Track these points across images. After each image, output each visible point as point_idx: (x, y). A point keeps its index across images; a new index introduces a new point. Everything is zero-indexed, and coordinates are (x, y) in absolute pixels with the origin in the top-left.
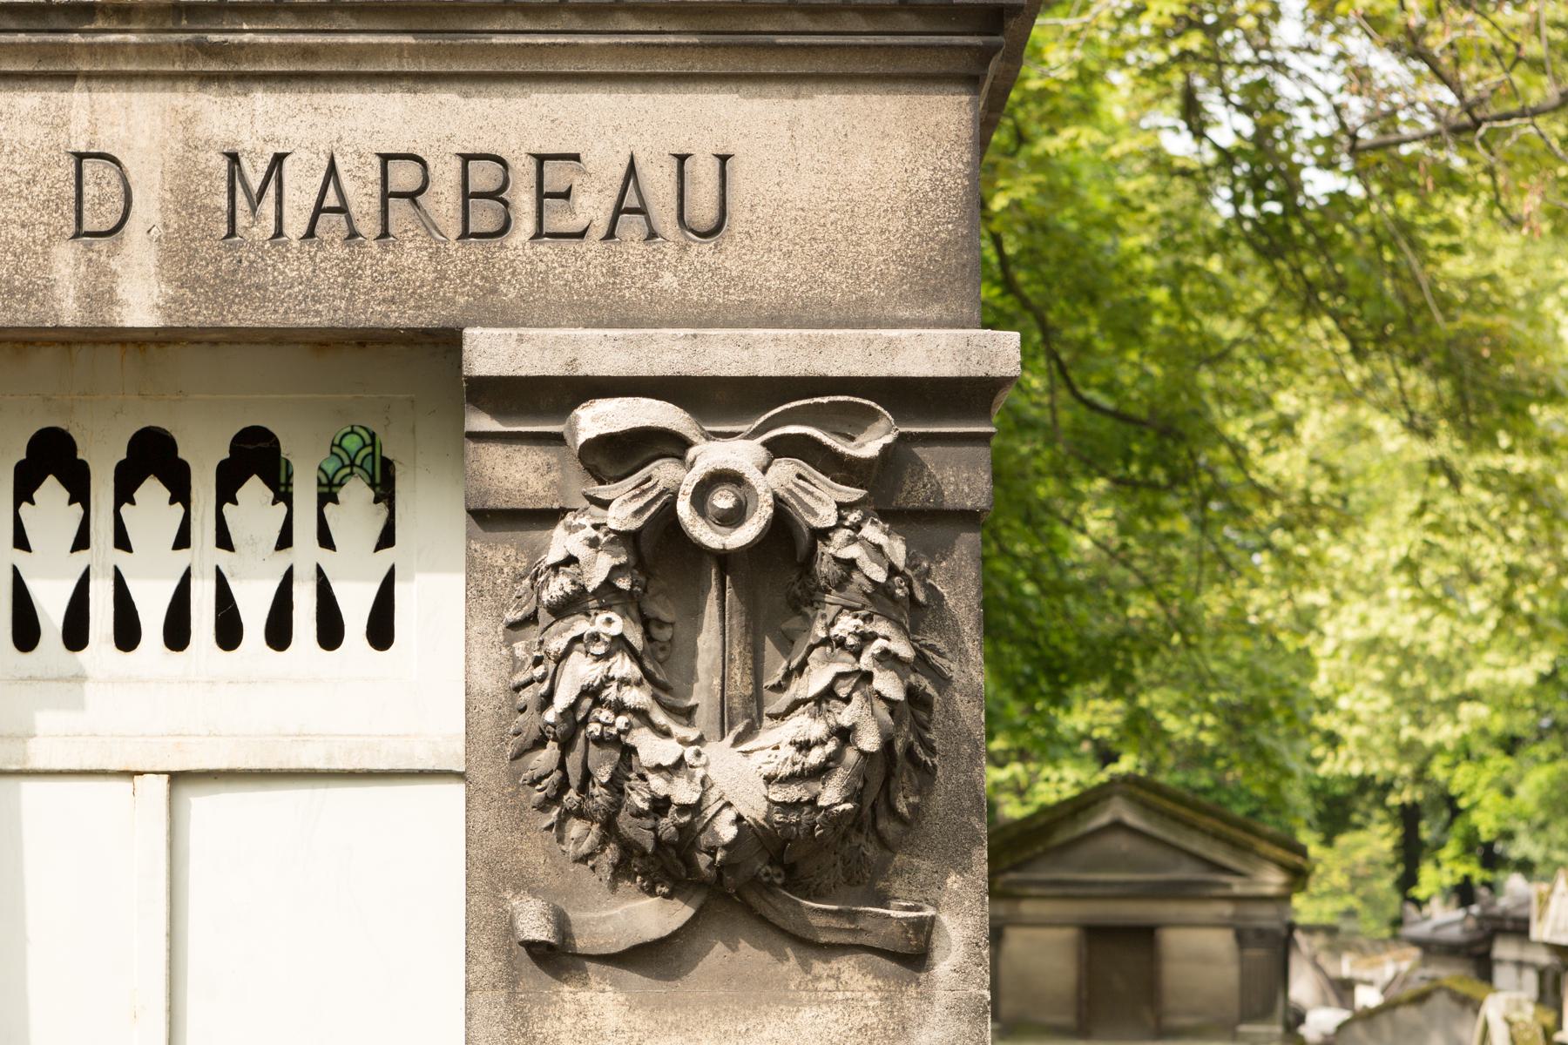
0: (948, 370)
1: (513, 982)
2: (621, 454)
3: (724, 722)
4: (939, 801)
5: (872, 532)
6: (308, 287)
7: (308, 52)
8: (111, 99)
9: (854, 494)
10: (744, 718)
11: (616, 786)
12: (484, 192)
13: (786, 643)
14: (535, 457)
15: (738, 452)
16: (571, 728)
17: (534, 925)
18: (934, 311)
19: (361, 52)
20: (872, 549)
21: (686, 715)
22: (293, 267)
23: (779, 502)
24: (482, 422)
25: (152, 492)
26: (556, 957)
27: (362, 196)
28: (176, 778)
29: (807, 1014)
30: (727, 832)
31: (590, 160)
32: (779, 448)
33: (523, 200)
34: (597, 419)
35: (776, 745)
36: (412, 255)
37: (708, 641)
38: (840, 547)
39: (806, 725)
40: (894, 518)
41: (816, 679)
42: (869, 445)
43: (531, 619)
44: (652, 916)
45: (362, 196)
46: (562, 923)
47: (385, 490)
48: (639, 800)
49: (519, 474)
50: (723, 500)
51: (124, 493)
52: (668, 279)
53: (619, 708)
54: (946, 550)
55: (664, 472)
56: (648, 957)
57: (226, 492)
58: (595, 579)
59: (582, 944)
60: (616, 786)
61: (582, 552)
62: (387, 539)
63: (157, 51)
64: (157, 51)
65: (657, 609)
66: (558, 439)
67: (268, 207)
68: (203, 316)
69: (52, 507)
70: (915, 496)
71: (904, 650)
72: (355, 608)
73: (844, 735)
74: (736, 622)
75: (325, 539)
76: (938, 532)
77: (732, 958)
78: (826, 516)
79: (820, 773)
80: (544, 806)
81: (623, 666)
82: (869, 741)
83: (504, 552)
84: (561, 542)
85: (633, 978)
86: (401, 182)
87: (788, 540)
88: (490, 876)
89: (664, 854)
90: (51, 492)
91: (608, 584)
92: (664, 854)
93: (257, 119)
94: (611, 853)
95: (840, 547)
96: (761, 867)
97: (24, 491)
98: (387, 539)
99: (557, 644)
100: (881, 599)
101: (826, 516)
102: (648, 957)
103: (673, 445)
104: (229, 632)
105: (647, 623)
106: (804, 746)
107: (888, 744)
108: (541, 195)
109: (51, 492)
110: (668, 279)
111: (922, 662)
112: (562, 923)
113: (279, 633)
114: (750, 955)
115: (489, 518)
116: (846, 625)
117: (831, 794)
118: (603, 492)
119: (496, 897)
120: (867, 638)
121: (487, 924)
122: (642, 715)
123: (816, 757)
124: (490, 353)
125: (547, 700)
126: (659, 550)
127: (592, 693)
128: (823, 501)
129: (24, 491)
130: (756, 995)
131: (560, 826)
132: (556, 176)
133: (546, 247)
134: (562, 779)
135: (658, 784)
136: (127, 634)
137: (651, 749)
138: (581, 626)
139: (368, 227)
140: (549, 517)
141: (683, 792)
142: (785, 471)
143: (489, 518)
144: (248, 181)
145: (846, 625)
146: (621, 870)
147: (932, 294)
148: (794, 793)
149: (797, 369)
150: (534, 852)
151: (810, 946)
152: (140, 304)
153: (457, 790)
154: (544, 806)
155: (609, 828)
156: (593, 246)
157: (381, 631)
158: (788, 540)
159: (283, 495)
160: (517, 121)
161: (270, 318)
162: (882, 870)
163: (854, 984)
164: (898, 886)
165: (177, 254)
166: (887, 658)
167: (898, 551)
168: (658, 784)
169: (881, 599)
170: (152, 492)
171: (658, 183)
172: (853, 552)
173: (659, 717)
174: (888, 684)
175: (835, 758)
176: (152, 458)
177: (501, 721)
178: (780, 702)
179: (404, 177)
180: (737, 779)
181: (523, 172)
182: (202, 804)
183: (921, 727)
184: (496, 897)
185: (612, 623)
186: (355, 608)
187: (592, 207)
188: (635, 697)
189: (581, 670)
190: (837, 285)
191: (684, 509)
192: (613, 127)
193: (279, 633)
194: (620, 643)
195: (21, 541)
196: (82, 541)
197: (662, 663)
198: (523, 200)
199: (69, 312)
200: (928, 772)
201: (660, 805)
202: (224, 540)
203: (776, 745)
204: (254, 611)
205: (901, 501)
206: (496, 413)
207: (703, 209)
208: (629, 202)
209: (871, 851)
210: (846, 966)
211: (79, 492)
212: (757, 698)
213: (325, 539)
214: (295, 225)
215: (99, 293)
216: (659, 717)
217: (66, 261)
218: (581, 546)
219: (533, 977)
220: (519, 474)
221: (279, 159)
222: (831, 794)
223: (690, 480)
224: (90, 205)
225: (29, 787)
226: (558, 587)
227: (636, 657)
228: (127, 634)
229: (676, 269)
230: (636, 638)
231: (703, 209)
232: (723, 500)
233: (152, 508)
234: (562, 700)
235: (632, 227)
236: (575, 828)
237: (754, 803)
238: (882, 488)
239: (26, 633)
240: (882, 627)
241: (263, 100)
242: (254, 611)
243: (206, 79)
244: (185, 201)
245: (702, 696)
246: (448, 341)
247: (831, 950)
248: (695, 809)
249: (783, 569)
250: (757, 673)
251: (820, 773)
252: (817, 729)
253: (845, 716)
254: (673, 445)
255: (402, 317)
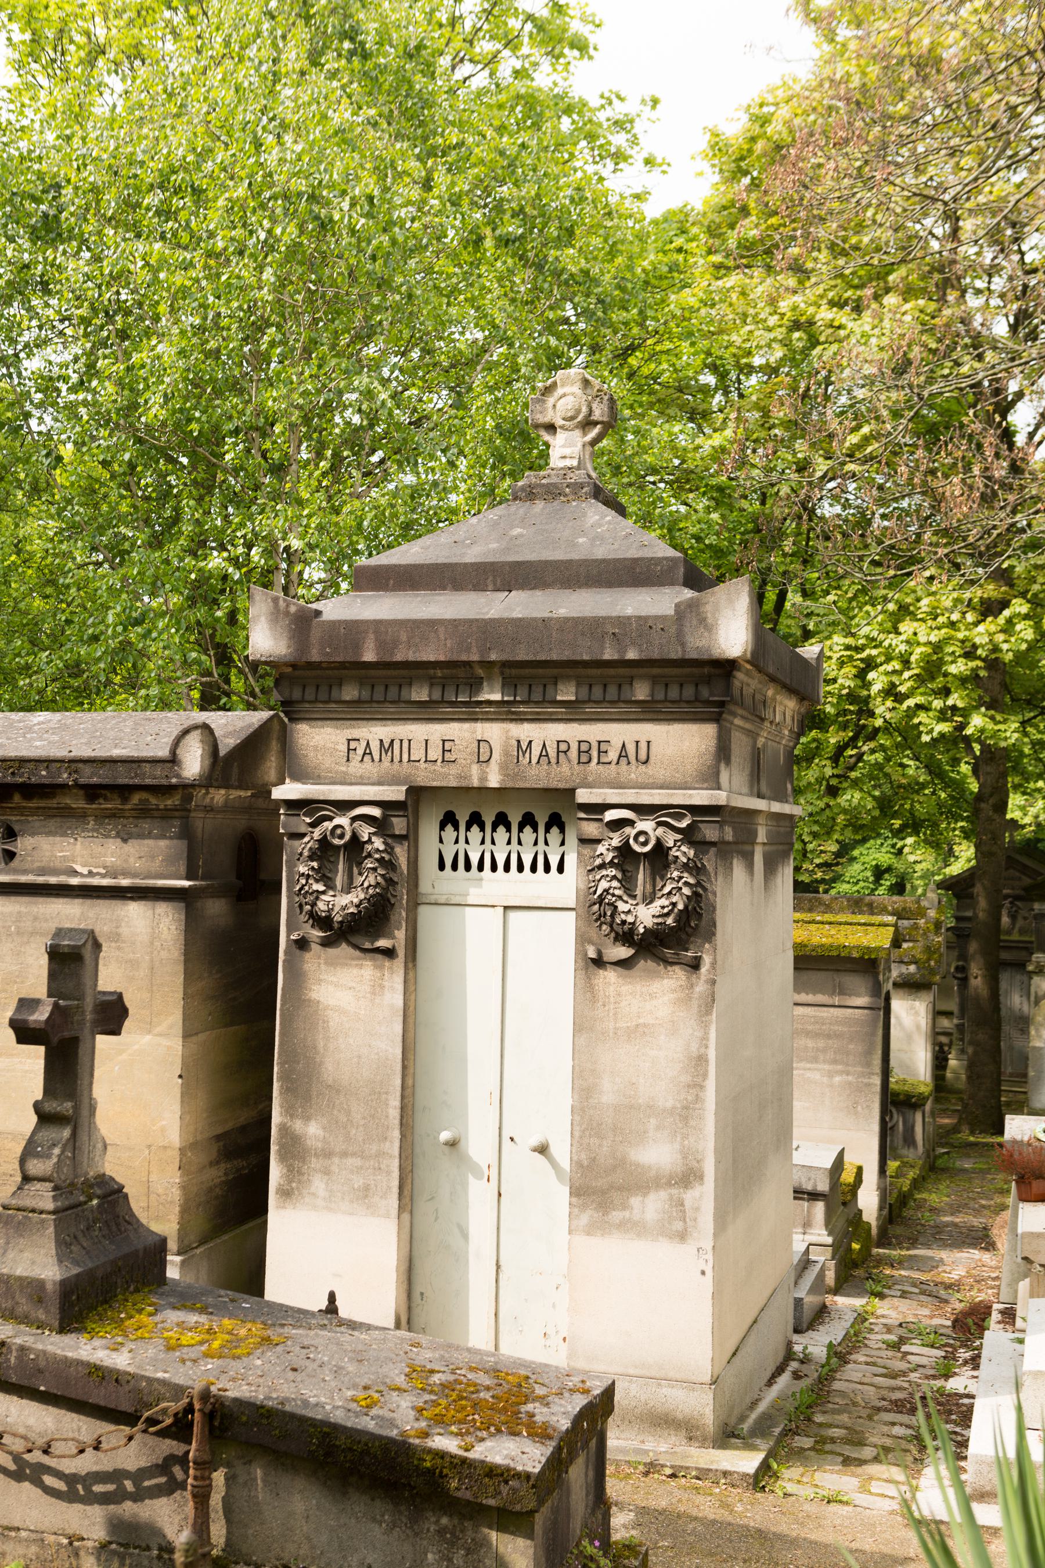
0: (706, 803)
1: (587, 969)
2: (617, 825)
3: (644, 899)
4: (703, 923)
5: (684, 848)
6: (537, 776)
7: (538, 713)
8: (487, 725)
9: (680, 837)
10: (649, 899)
11: (612, 916)
12: (584, 752)
13: (662, 878)
14: (596, 824)
15: (646, 825)
16: (601, 900)
17: (592, 954)
18: (705, 785)
19: (551, 713)
20: (684, 853)
21: (634, 897)
22: (534, 771)
23: (658, 840)
24: (582, 815)
25: (501, 829)
26: (599, 962)
27: (552, 752)
28: (506, 908)
29: (666, 981)
30: (642, 930)
31: (613, 743)
32: (660, 824)
33: (594, 753)
34: (610, 815)
35: (656, 907)
36: (565, 768)
37: (641, 876)
38: (674, 852)
39: (664, 902)
40: (691, 843)
41: (666, 890)
42: (684, 824)
43: (593, 869)
44: (624, 952)
45: (552, 752)
46: (600, 953)
47: (562, 830)
48: (618, 921)
49: (591, 829)
50: (642, 839)
51: (521, 830)
52: (633, 776)
53: (613, 895)
54: (707, 852)
55: (628, 830)
56: (623, 964)
57: (521, 830)
58: (608, 860)
59: (605, 959)
60: (612, 916)
61: (605, 852)
62: (563, 844)
63: (499, 713)
64: (499, 713)
65: (628, 867)
66: (601, 820)
67: (527, 755)
68: (510, 785)
69: (449, 832)
70: (698, 837)
71: (692, 881)
72: (554, 863)
73: (674, 904)
74: (648, 872)
75: (546, 843)
76: (705, 847)
77: (645, 965)
78: (671, 844)
79: (667, 915)
80: (596, 920)
81: (615, 884)
82: (680, 906)
83: (587, 851)
84: (601, 849)
85: (619, 969)
86: (562, 749)
87: (660, 849)
88: (582, 940)
89: (626, 935)
90: (449, 828)
91: (612, 861)
92: (626, 935)
93: (526, 731)
94: (613, 935)
95: (674, 852)
96: (652, 940)
97: (442, 827)
98: (563, 844)
99: (598, 877)
100: (686, 867)
101: (671, 844)
102: (623, 964)
103: (630, 823)
104: (520, 868)
105: (624, 872)
106: (663, 907)
107: (686, 907)
108: (599, 752)
109: (449, 828)
110: (633, 776)
111: (699, 884)
112: (600, 953)
113: (534, 869)
114: (650, 964)
115: (584, 841)
116: (675, 874)
117: (670, 921)
118: (611, 835)
119: (583, 946)
120: (681, 878)
121: (580, 952)
122: (620, 898)
123: (666, 910)
124: (583, 796)
125: (595, 892)
126: (624, 851)
127: (606, 891)
128: (670, 839)
129: (442, 827)
130: (653, 975)
131: (600, 926)
132: (603, 747)
133: (600, 766)
134: (598, 911)
135: (623, 916)
136: (494, 868)
137: (622, 907)
138: (604, 872)
139: (553, 761)
140: (598, 841)
141: (630, 919)
142: (660, 831)
143: (584, 841)
144: (522, 748)
145: (675, 874)
146: (616, 939)
147: (705, 781)
148: (660, 920)
149: (665, 802)
150: (593, 933)
151: (667, 963)
152: (494, 781)
153: (573, 914)
154: (596, 920)
155: (612, 929)
156: (613, 766)
157: (561, 869)
158: (660, 849)
159: (536, 830)
160: (593, 732)
161: (528, 785)
162: (687, 942)
163: (678, 974)
164: (691, 946)
165: (503, 767)
166: (686, 884)
167: (691, 853)
168: (623, 916)
169: (686, 867)
170: (501, 829)
171: (631, 749)
172: (678, 854)
173: (625, 898)
174: (686, 891)
175: (672, 911)
176: (502, 820)
177: (586, 897)
178: (659, 894)
179: (563, 747)
180: (645, 916)
181: (595, 745)
182: (512, 915)
183: (698, 902)
184: (583, 946)
185: (612, 872)
186: (554, 863)
187: (613, 755)
188: (617, 892)
189: (604, 885)
190: (679, 778)
191: (631, 841)
192: (618, 734)
193: (534, 869)
194: (614, 877)
195: (441, 841)
196: (483, 842)
197: (628, 884)
198: (594, 753)
199: (476, 783)
200: (701, 915)
201: (624, 922)
202: (520, 843)
203: (656, 907)
204: (527, 863)
205: (694, 839)
206: (585, 812)
207: (643, 756)
208: (544, 754)
209: (684, 936)
210: (677, 968)
211: (482, 829)
212: (654, 893)
213: (546, 843)
214: (534, 760)
215: (483, 778)
216: (625, 898)
217: (475, 769)
218: (604, 851)
219: (592, 967)
220: (591, 829)
221: (392, 741)
222: (670, 921)
223: (634, 832)
224: (482, 752)
225: (467, 909)
226: (599, 861)
227: (619, 881)
228: (494, 868)
229: (634, 772)
230: (619, 876)
231: (643, 756)
232: (642, 839)
233: (501, 833)
234: (599, 892)
235: (623, 760)
236: (604, 927)
237: (649, 922)
238: (688, 835)
239: (442, 866)
240: (685, 875)
241: (526, 726)
242: (527, 863)
243: (512, 720)
244: (506, 753)
245: (639, 892)
246: (572, 792)
247: (672, 964)
248: (633, 923)
249: (659, 857)
250: (654, 886)
251: (667, 915)
252: (667, 903)
253: (674, 899)
254: (630, 823)
255: (561, 785)
